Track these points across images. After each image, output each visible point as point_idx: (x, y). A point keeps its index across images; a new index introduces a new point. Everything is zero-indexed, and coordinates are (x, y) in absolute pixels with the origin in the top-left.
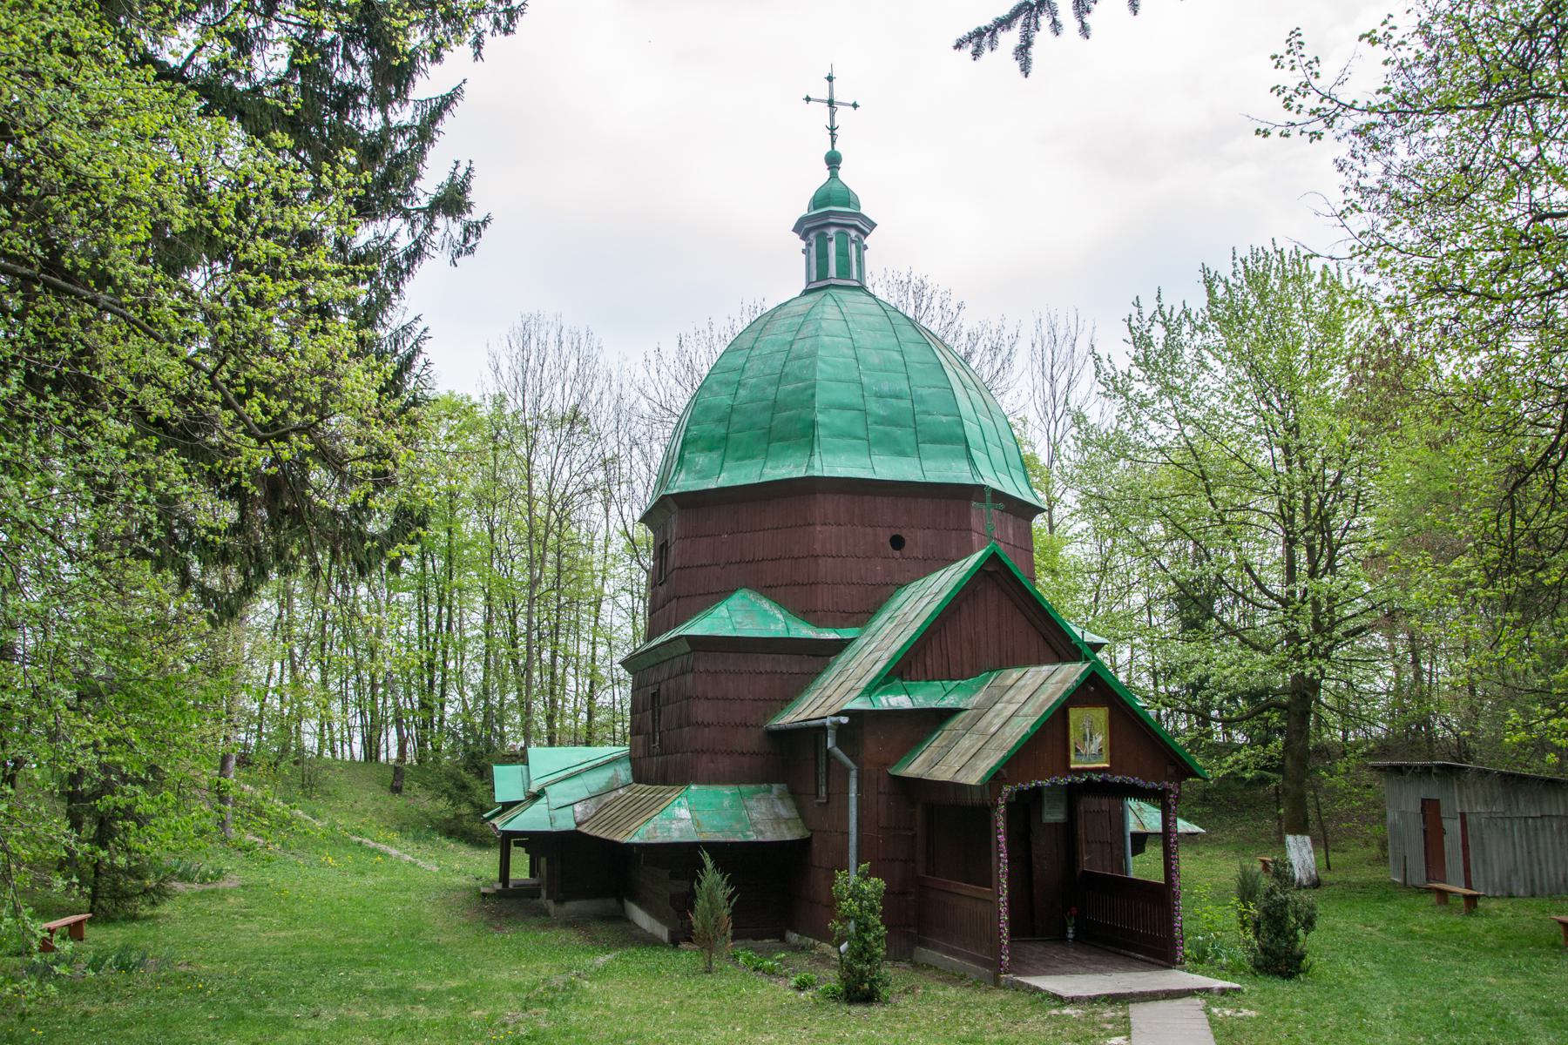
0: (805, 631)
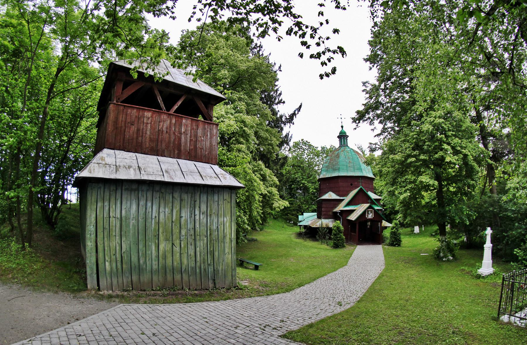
0: (338, 198)
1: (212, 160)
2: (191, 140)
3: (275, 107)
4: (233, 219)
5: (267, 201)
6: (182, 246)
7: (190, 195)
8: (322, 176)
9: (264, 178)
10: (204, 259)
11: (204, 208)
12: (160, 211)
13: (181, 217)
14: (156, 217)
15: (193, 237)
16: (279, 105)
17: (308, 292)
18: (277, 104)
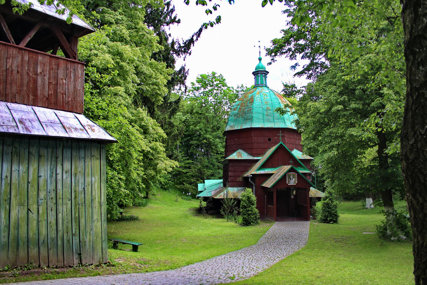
0: (251, 158)
1: (76, 108)
2: (50, 83)
3: (165, 28)
4: (103, 179)
5: (148, 160)
6: (41, 211)
7: (50, 151)
8: (228, 128)
9: (145, 131)
10: (67, 228)
11: (67, 166)
12: (13, 169)
13: (39, 177)
14: (7, 177)
15: (54, 201)
16: (171, 25)
17: (197, 269)
18: (168, 24)
